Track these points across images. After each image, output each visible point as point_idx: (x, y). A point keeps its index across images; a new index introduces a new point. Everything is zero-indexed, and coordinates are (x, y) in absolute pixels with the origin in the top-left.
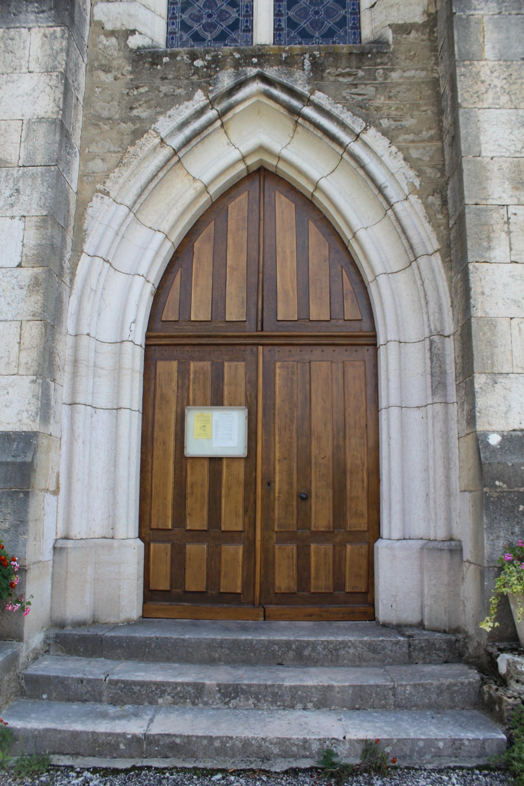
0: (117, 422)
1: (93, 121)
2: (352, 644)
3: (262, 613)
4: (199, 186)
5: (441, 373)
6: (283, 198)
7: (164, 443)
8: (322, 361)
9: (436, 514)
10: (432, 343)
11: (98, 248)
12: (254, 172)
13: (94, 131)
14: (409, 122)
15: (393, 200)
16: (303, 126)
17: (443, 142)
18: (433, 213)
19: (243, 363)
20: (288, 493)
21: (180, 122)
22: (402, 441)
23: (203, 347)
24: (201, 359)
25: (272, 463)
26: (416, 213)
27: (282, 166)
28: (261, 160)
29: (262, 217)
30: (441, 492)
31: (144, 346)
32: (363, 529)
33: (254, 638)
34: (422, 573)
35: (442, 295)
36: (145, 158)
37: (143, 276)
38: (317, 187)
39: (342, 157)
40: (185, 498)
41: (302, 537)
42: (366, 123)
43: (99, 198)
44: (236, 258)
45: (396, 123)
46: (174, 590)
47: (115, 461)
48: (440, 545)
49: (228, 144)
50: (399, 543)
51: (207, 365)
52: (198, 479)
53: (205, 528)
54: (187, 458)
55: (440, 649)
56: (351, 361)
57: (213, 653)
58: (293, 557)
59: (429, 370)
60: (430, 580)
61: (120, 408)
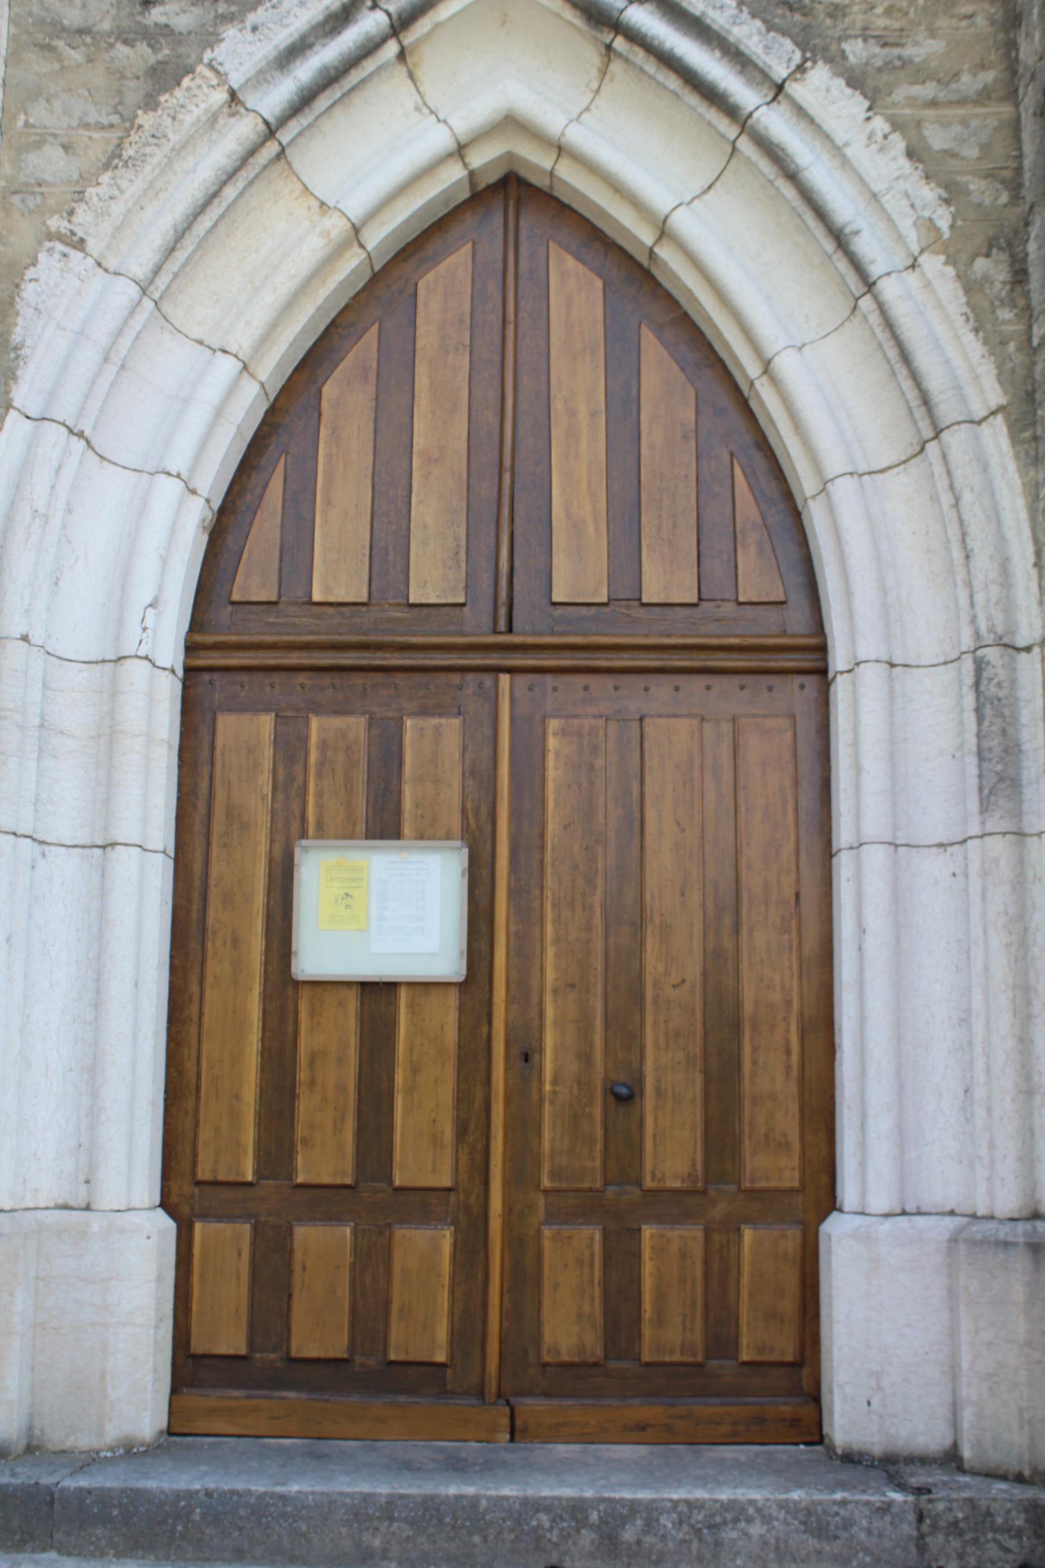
0: (103, 883)
1: (40, 36)
2: (758, 1510)
3: (505, 1421)
4: (336, 226)
5: (1006, 751)
6: (571, 262)
7: (236, 942)
8: (676, 716)
9: (992, 1145)
10: (980, 667)
11: (52, 396)
12: (490, 188)
13: (38, 65)
14: (924, 48)
15: (875, 270)
16: (627, 61)
17: (1017, 105)
18: (986, 304)
19: (456, 722)
20: (579, 1083)
21: (283, 46)
22: (898, 939)
23: (346, 675)
24: (340, 711)
25: (535, 1000)
26: (940, 305)
27: (567, 173)
28: (510, 156)
29: (511, 316)
30: (1006, 1082)
31: (180, 673)
32: (788, 1185)
33: (483, 1492)
34: (953, 1310)
35: (1011, 534)
36: (184, 146)
37: (178, 476)
38: (664, 231)
39: (734, 149)
40: (293, 1097)
41: (618, 1206)
42: (804, 51)
43: (57, 256)
44: (440, 431)
45: (887, 50)
46: (258, 1355)
47: (98, 992)
48: (1004, 1232)
49: (417, 109)
50: (888, 1225)
51: (356, 726)
52: (330, 1042)
53: (348, 1181)
54: (298, 984)
55: (1006, 1529)
56: (754, 716)
57: (365, 1537)
58: (592, 1262)
59: (972, 741)
60: (977, 1331)
61: (113, 845)
